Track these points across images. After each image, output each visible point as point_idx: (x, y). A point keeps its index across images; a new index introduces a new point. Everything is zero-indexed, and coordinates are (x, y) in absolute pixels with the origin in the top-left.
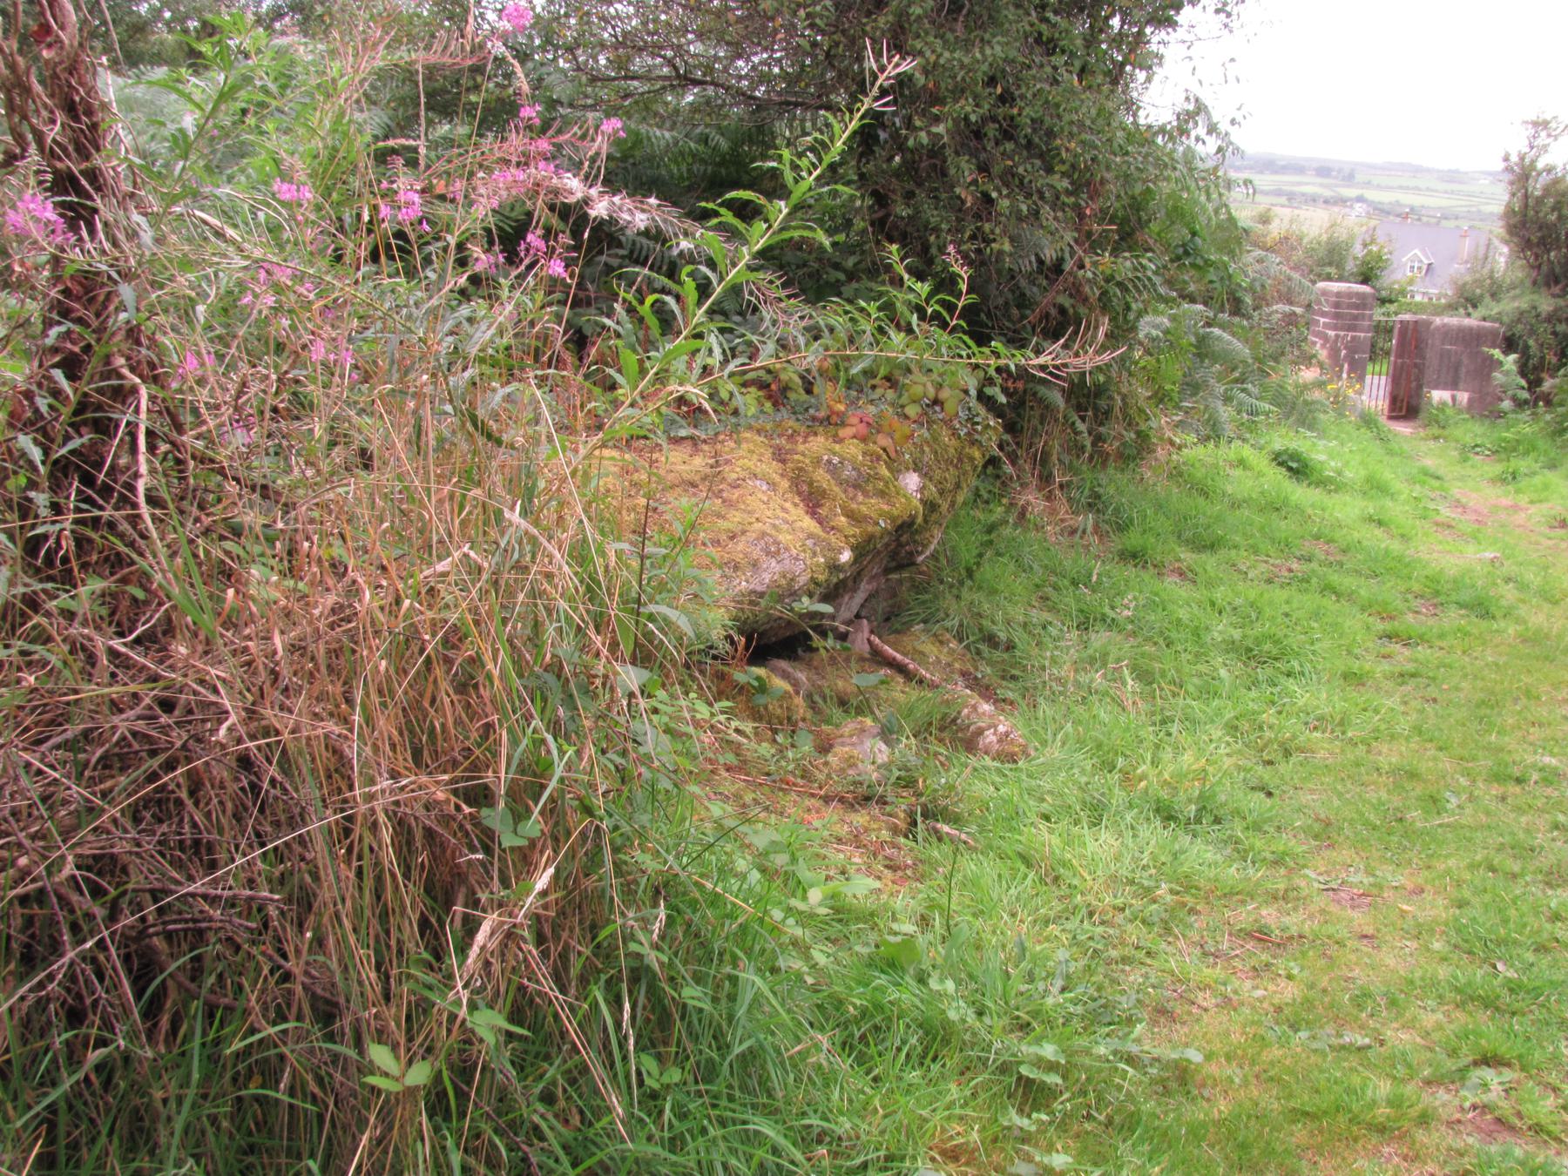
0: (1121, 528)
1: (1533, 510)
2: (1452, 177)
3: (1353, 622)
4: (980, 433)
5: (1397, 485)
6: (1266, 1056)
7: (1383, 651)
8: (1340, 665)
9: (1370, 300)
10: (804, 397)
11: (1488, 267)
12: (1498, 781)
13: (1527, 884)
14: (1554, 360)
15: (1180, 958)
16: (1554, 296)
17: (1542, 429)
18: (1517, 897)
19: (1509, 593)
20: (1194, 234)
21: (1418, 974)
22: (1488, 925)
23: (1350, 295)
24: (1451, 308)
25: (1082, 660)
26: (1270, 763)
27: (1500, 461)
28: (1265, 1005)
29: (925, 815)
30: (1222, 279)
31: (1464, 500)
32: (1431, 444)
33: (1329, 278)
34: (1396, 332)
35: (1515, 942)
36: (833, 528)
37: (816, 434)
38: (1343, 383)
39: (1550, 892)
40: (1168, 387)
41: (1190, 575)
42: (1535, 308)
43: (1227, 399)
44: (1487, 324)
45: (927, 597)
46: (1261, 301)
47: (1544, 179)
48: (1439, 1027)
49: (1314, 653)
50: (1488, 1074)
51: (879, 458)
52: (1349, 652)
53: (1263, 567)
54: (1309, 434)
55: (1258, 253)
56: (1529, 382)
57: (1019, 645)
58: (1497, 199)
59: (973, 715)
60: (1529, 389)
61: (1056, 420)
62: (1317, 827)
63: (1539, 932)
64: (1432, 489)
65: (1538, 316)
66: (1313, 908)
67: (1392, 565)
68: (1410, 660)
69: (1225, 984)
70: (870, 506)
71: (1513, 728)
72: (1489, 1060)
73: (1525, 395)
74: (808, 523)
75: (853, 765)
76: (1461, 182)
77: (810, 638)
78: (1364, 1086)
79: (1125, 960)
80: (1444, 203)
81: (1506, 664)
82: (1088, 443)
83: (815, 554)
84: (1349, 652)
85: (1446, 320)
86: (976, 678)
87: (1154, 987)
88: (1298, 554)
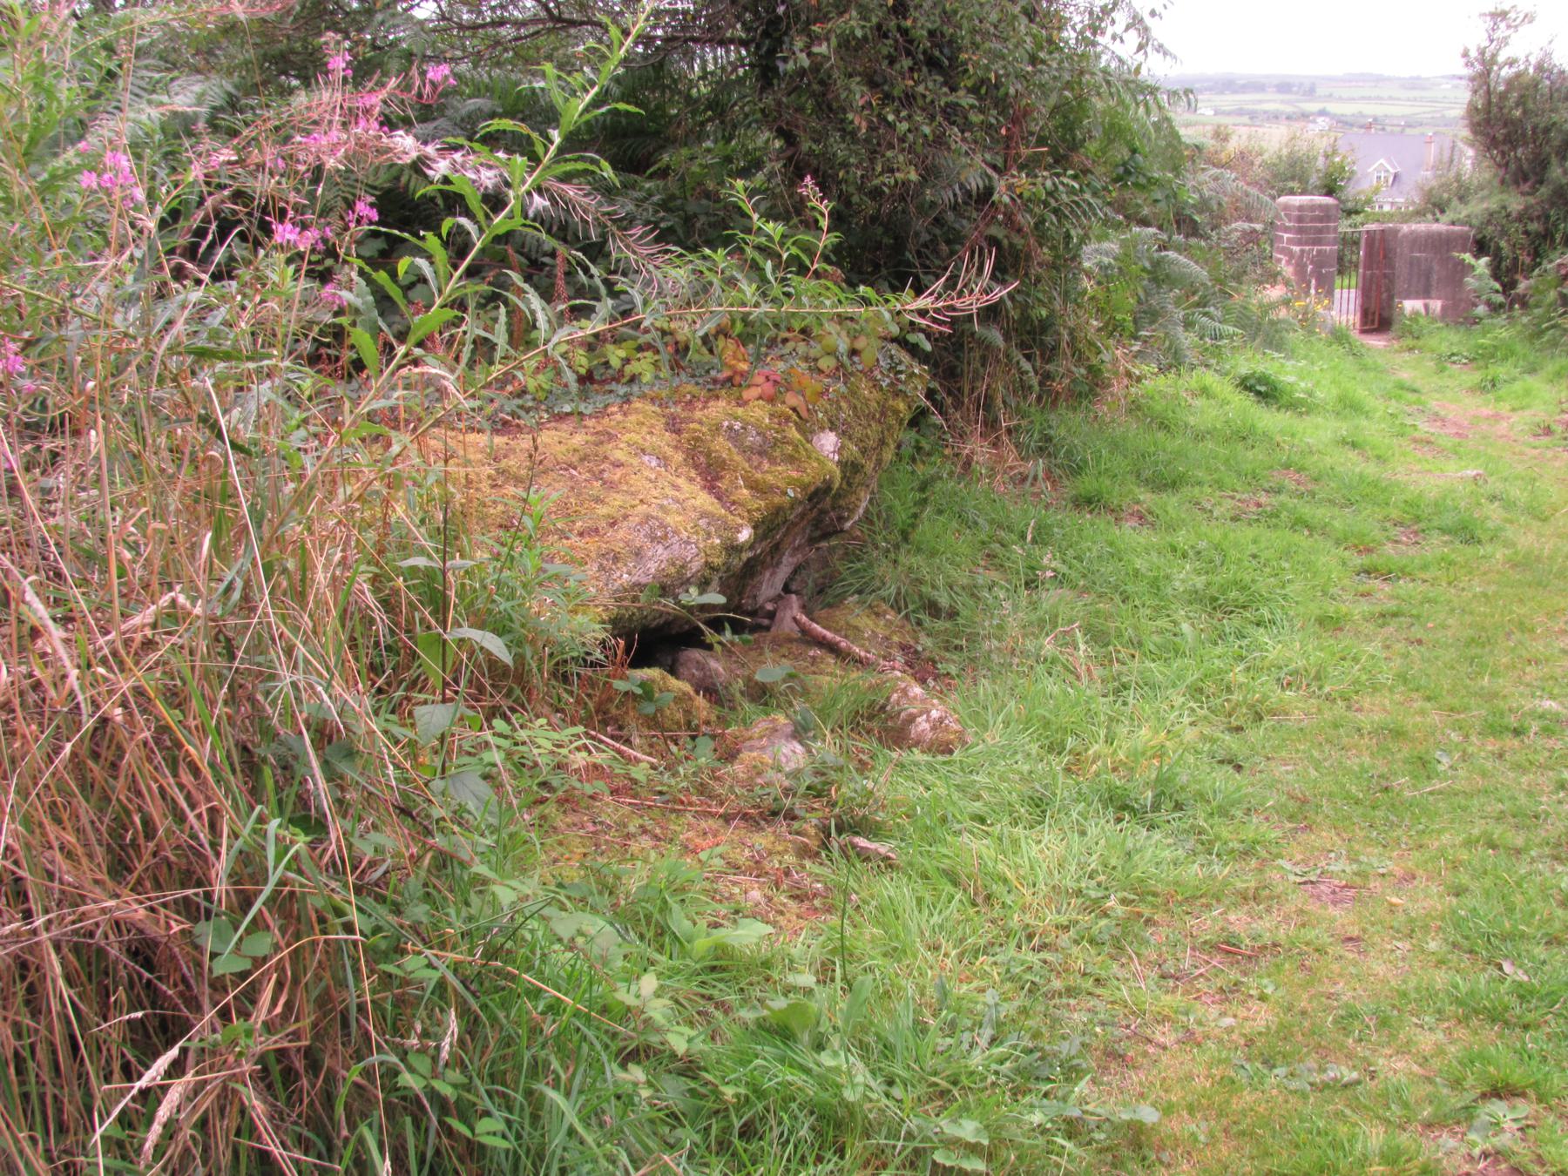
0: (1077, 470)
1: (1515, 418)
2: (1414, 84)
4: (904, 383)
5: (1372, 402)
6: (1236, 1105)
7: (1361, 589)
8: (1314, 609)
9: (1334, 212)
10: (707, 357)
12: (1493, 734)
13: (1533, 861)
14: (1528, 260)
15: (1136, 986)
16: (1523, 194)
17: (1519, 333)
18: (1523, 878)
19: (1494, 512)
20: (1134, 151)
21: (1412, 983)
22: (1490, 917)
23: (1313, 208)
24: (1419, 214)
25: (1031, 623)
26: (1239, 729)
27: (1479, 369)
28: (1234, 1036)
29: (840, 831)
31: (1443, 413)
32: (1406, 356)
33: (1292, 192)
35: (1523, 936)
36: (734, 503)
37: (717, 398)
38: (1312, 298)
39: (1560, 869)
41: (1150, 518)
42: (1504, 208)
43: (1188, 324)
44: (1457, 228)
45: (858, 565)
46: (1218, 220)
47: (1506, 72)
48: (1440, 1051)
49: (1285, 597)
50: (1498, 1108)
51: (788, 419)
52: (1325, 593)
53: (1229, 503)
54: (1276, 355)
55: (1214, 171)
56: (1504, 286)
58: (1457, 100)
59: (904, 701)
60: (1504, 293)
61: (998, 361)
62: (1292, 806)
63: (1550, 920)
65: (1508, 215)
66: (1289, 907)
68: (1392, 597)
69: (1187, 1014)
70: (778, 474)
71: (1507, 667)
72: (1500, 1091)
73: (1500, 298)
74: (704, 500)
75: (759, 774)
76: (1424, 89)
77: (702, 633)
78: (1352, 1138)
79: (1070, 992)
81: (1496, 593)
83: (709, 535)
84: (1325, 593)
85: (1414, 227)
86: (916, 652)
87: (1103, 1024)
88: (1266, 486)
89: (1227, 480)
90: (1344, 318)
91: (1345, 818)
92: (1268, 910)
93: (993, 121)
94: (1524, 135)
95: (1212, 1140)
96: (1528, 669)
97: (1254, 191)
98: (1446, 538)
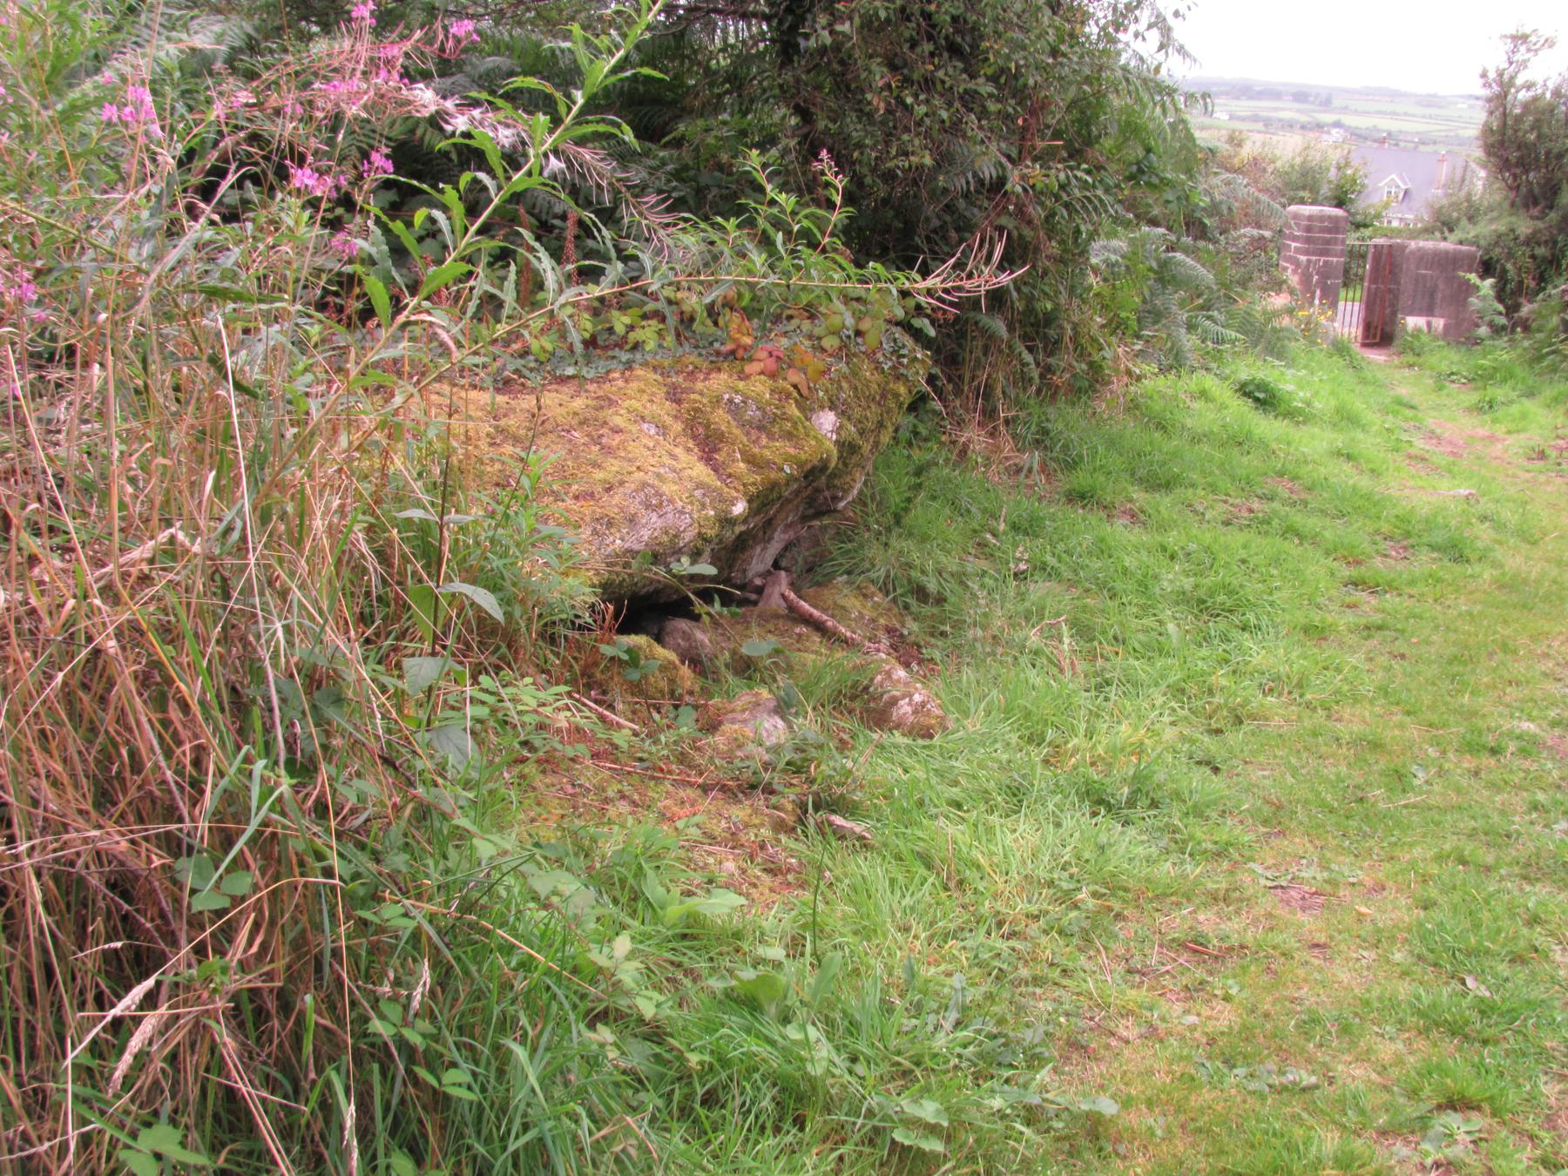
0: (1071, 465)
1: (1510, 440)
2: (1430, 101)
3: (1318, 569)
4: (906, 367)
6: (1194, 1102)
7: (1348, 600)
8: (1300, 617)
9: (1342, 224)
11: (1466, 189)
12: (1470, 751)
14: (1532, 284)
15: (1101, 979)
16: (1532, 218)
17: (1519, 356)
18: (1491, 895)
19: (1484, 533)
20: (1149, 150)
22: (1457, 932)
23: (1322, 218)
24: (1428, 231)
26: (1218, 732)
27: (1477, 389)
28: (1197, 1035)
29: (817, 808)
30: (1178, 198)
31: (1438, 431)
33: (1302, 202)
34: (1370, 257)
35: (1487, 952)
36: (730, 476)
37: (719, 370)
38: (1315, 310)
39: (1528, 888)
40: (1123, 315)
42: (1513, 230)
43: (1191, 327)
44: (1464, 248)
45: (850, 546)
46: (1227, 225)
47: (1523, 95)
48: (1399, 1061)
50: (1453, 1120)
51: (788, 396)
53: (1221, 507)
54: (1277, 363)
56: (1507, 308)
57: (952, 599)
58: (1473, 120)
60: (1507, 315)
61: (1001, 351)
62: (1267, 811)
64: (1406, 420)
65: (1516, 239)
66: (1259, 910)
67: (1360, 503)
68: (1377, 610)
70: (775, 450)
71: (1487, 686)
73: (1502, 321)
74: (701, 471)
76: (1440, 107)
77: (691, 603)
78: (1307, 1142)
79: (1037, 981)
80: (1421, 127)
82: (1035, 374)
83: (703, 506)
85: (1421, 244)
86: (902, 635)
87: (1067, 1015)
88: (1259, 492)
89: (1220, 484)
90: (1346, 330)
91: (1319, 826)
92: (1238, 912)
93: (1010, 110)
95: (1169, 1136)
96: (1508, 690)
97: (1264, 198)
98: (1435, 555)
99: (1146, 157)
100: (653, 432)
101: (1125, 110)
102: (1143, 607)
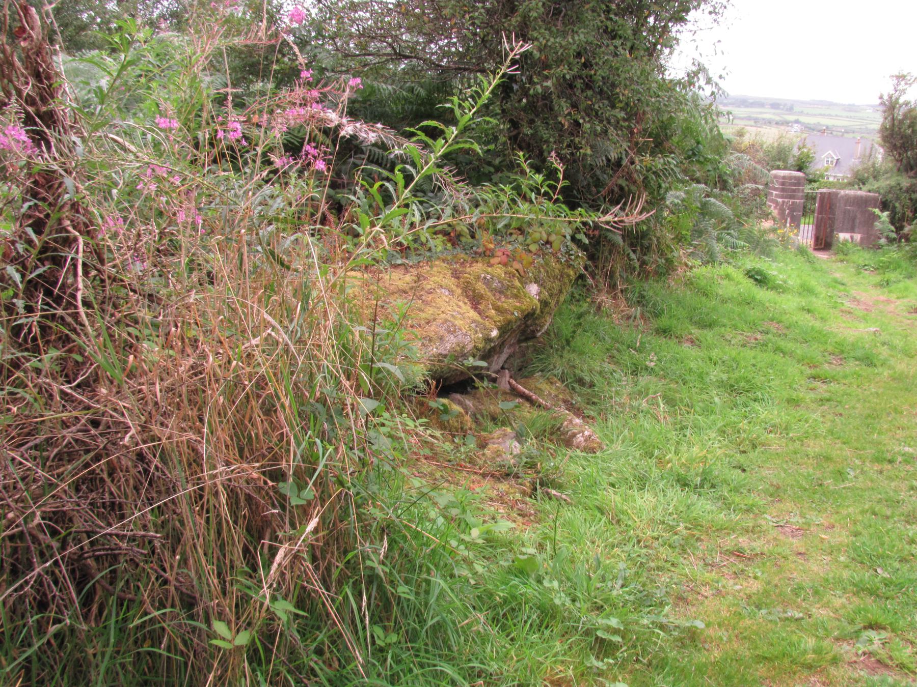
0: (657, 315)
2: (851, 108)
3: (794, 370)
5: (819, 289)
7: (810, 386)
8: (785, 394)
10: (470, 240)
12: (878, 462)
14: (911, 215)
15: (691, 567)
16: (910, 177)
18: (889, 530)
19: (884, 352)
20: (698, 143)
21: (831, 575)
23: (791, 178)
24: (851, 184)
26: (744, 452)
27: (879, 274)
29: (542, 484)
31: (858, 297)
32: (839, 264)
33: (778, 168)
34: (818, 199)
35: (888, 557)
36: (487, 317)
37: (477, 262)
39: (908, 527)
41: (697, 342)
42: (899, 184)
43: (719, 239)
44: (871, 194)
45: (543, 356)
46: (738, 182)
47: (903, 110)
50: (872, 634)
51: (514, 276)
52: (791, 387)
53: (740, 337)
54: (767, 259)
56: (896, 228)
58: (876, 121)
62: (772, 490)
66: (770, 537)
67: (816, 335)
68: (827, 391)
69: (717, 582)
70: (509, 303)
71: (887, 430)
72: (873, 626)
73: (894, 235)
74: (473, 314)
76: (856, 112)
77: (473, 381)
79: (659, 568)
82: (637, 265)
83: (476, 332)
84: (791, 387)
85: (847, 192)
86: (572, 404)
87: (676, 584)
88: (760, 329)
89: (739, 325)
90: (805, 241)
91: (799, 497)
92: (759, 538)
94: (912, 144)
95: (730, 640)
96: (898, 432)
97: (759, 167)
98: (857, 363)
99: (697, 147)
100: (447, 293)
101: (685, 121)
102: (701, 389)
